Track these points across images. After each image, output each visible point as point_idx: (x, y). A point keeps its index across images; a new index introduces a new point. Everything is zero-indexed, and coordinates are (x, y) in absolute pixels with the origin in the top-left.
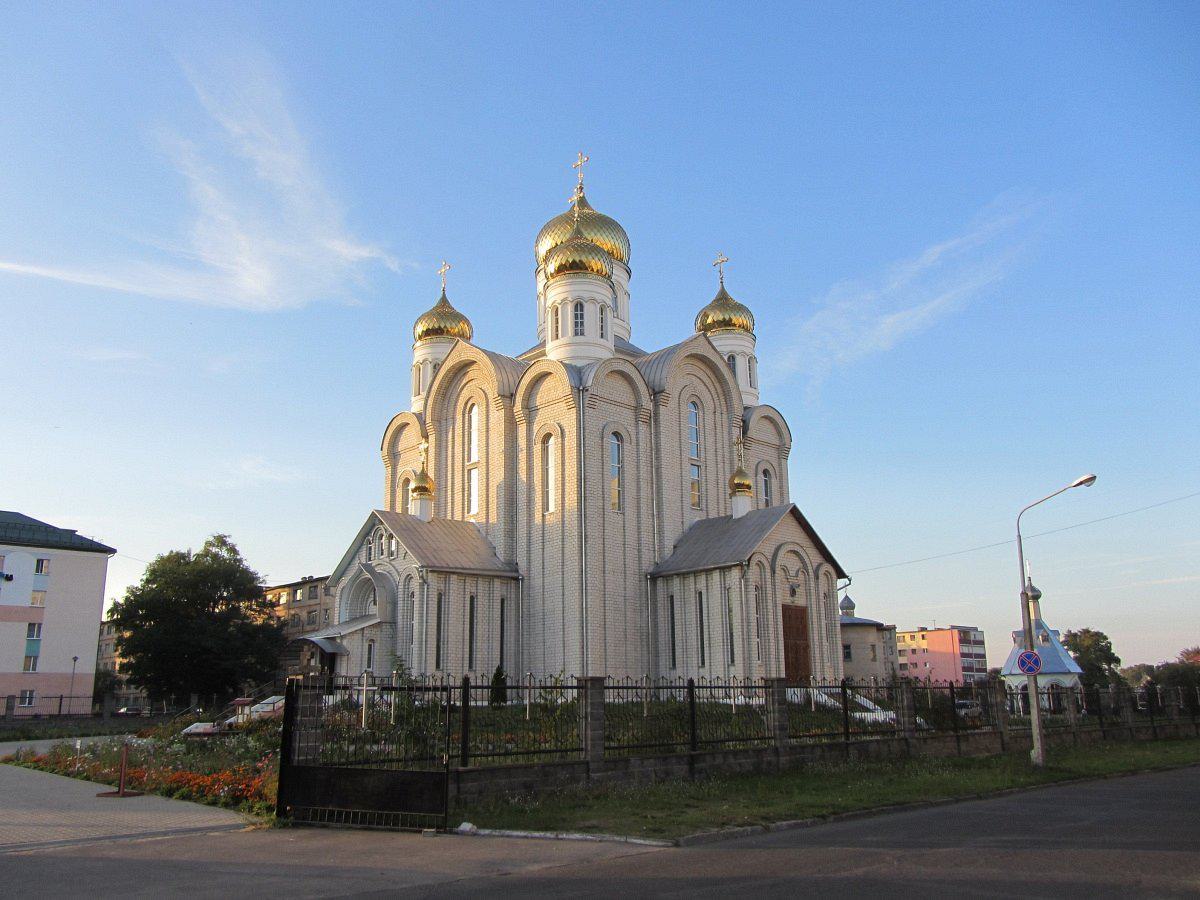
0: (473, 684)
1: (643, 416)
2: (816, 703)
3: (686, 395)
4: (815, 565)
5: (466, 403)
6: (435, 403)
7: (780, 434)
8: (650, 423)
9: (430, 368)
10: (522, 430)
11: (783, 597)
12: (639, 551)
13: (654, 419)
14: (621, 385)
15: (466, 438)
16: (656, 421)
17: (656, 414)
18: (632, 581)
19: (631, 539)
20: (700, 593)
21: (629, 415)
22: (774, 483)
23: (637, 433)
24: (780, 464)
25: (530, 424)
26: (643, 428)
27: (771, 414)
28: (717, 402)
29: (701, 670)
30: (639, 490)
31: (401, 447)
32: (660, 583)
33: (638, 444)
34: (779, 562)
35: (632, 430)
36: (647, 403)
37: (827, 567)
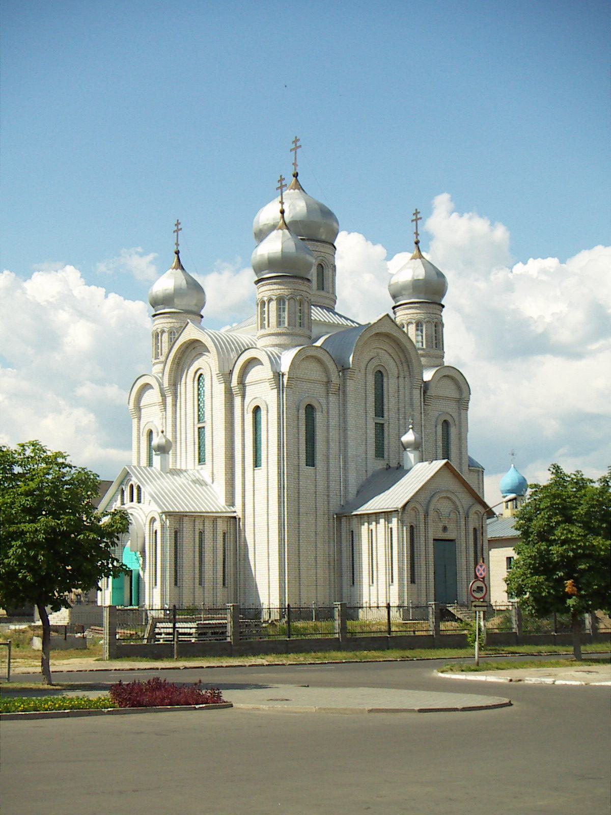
0: (292, 607)
1: (333, 389)
2: (559, 621)
3: (375, 362)
4: (466, 507)
5: (196, 373)
6: (171, 370)
7: (459, 388)
8: (339, 394)
9: (165, 337)
10: (238, 400)
11: (434, 531)
12: (328, 496)
13: (342, 391)
14: (314, 366)
15: (183, 498)
16: (344, 392)
17: (344, 386)
18: (322, 522)
19: (321, 488)
20: (200, 584)
21: (320, 390)
22: (453, 431)
23: (328, 403)
24: (460, 414)
25: (243, 397)
26: (333, 398)
27: (452, 373)
28: (400, 368)
29: (352, 588)
30: (328, 448)
31: (142, 404)
32: (344, 520)
33: (328, 413)
34: (432, 507)
35: (323, 401)
36: (335, 379)
37: (479, 508)
